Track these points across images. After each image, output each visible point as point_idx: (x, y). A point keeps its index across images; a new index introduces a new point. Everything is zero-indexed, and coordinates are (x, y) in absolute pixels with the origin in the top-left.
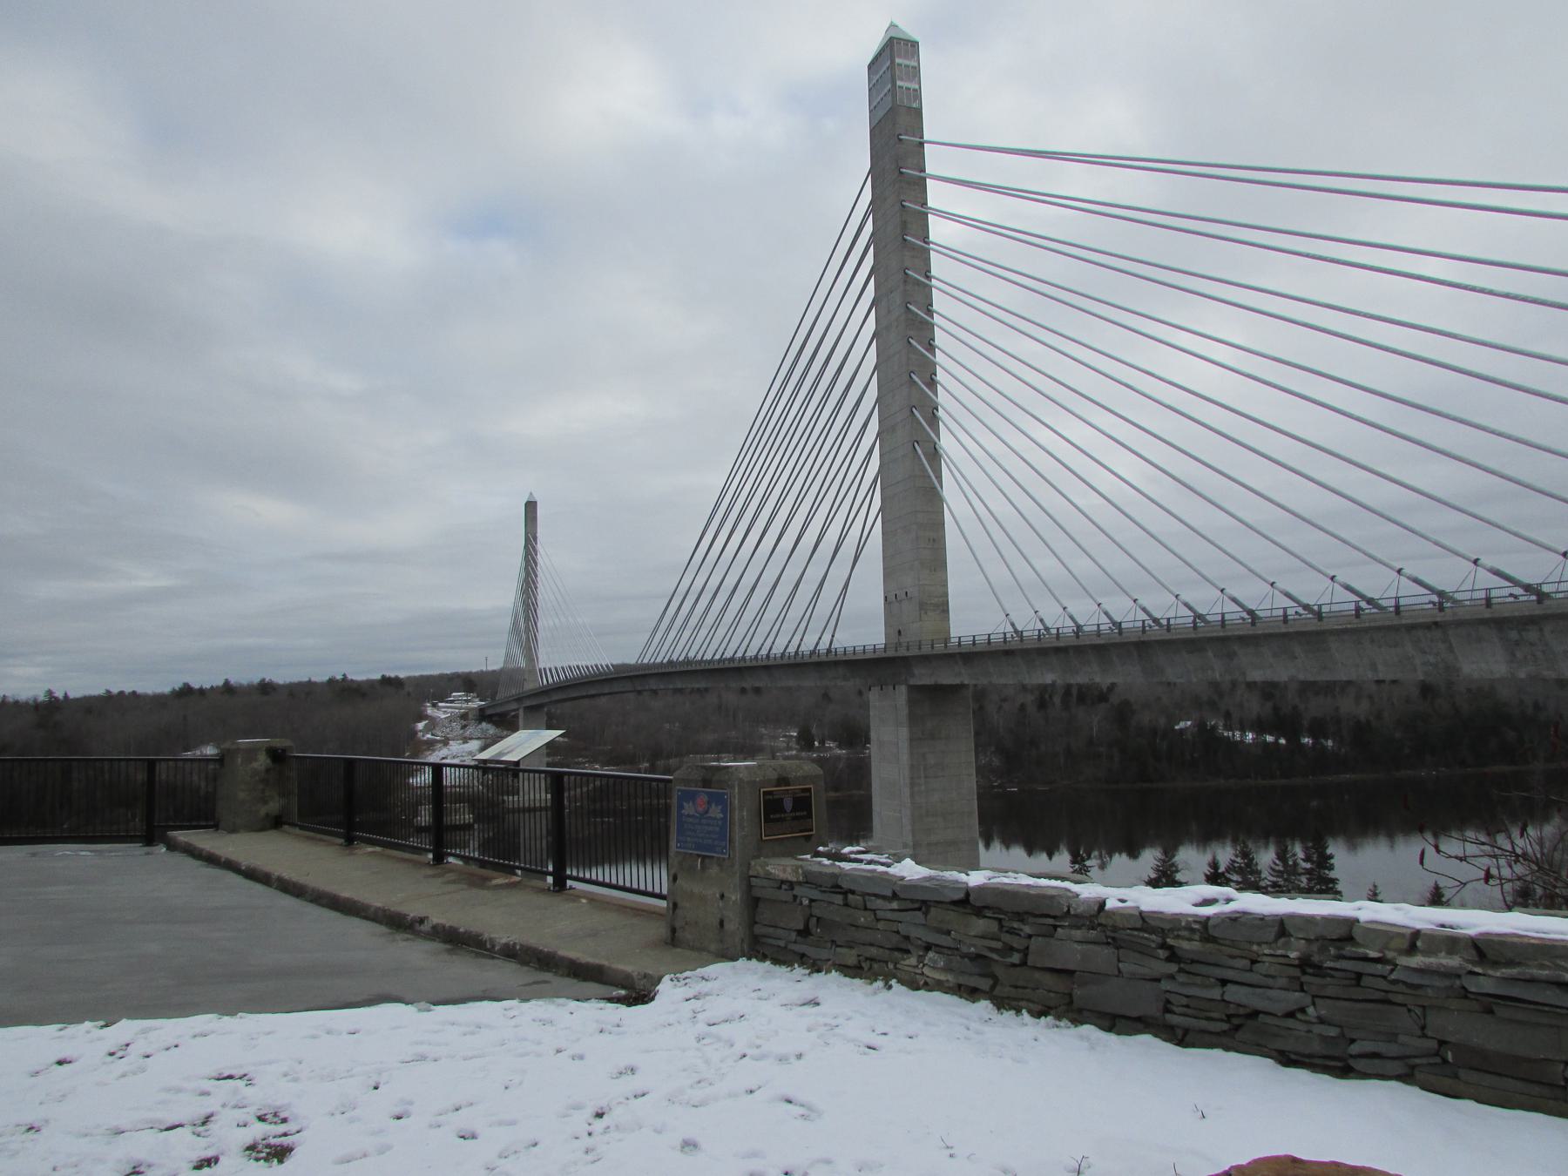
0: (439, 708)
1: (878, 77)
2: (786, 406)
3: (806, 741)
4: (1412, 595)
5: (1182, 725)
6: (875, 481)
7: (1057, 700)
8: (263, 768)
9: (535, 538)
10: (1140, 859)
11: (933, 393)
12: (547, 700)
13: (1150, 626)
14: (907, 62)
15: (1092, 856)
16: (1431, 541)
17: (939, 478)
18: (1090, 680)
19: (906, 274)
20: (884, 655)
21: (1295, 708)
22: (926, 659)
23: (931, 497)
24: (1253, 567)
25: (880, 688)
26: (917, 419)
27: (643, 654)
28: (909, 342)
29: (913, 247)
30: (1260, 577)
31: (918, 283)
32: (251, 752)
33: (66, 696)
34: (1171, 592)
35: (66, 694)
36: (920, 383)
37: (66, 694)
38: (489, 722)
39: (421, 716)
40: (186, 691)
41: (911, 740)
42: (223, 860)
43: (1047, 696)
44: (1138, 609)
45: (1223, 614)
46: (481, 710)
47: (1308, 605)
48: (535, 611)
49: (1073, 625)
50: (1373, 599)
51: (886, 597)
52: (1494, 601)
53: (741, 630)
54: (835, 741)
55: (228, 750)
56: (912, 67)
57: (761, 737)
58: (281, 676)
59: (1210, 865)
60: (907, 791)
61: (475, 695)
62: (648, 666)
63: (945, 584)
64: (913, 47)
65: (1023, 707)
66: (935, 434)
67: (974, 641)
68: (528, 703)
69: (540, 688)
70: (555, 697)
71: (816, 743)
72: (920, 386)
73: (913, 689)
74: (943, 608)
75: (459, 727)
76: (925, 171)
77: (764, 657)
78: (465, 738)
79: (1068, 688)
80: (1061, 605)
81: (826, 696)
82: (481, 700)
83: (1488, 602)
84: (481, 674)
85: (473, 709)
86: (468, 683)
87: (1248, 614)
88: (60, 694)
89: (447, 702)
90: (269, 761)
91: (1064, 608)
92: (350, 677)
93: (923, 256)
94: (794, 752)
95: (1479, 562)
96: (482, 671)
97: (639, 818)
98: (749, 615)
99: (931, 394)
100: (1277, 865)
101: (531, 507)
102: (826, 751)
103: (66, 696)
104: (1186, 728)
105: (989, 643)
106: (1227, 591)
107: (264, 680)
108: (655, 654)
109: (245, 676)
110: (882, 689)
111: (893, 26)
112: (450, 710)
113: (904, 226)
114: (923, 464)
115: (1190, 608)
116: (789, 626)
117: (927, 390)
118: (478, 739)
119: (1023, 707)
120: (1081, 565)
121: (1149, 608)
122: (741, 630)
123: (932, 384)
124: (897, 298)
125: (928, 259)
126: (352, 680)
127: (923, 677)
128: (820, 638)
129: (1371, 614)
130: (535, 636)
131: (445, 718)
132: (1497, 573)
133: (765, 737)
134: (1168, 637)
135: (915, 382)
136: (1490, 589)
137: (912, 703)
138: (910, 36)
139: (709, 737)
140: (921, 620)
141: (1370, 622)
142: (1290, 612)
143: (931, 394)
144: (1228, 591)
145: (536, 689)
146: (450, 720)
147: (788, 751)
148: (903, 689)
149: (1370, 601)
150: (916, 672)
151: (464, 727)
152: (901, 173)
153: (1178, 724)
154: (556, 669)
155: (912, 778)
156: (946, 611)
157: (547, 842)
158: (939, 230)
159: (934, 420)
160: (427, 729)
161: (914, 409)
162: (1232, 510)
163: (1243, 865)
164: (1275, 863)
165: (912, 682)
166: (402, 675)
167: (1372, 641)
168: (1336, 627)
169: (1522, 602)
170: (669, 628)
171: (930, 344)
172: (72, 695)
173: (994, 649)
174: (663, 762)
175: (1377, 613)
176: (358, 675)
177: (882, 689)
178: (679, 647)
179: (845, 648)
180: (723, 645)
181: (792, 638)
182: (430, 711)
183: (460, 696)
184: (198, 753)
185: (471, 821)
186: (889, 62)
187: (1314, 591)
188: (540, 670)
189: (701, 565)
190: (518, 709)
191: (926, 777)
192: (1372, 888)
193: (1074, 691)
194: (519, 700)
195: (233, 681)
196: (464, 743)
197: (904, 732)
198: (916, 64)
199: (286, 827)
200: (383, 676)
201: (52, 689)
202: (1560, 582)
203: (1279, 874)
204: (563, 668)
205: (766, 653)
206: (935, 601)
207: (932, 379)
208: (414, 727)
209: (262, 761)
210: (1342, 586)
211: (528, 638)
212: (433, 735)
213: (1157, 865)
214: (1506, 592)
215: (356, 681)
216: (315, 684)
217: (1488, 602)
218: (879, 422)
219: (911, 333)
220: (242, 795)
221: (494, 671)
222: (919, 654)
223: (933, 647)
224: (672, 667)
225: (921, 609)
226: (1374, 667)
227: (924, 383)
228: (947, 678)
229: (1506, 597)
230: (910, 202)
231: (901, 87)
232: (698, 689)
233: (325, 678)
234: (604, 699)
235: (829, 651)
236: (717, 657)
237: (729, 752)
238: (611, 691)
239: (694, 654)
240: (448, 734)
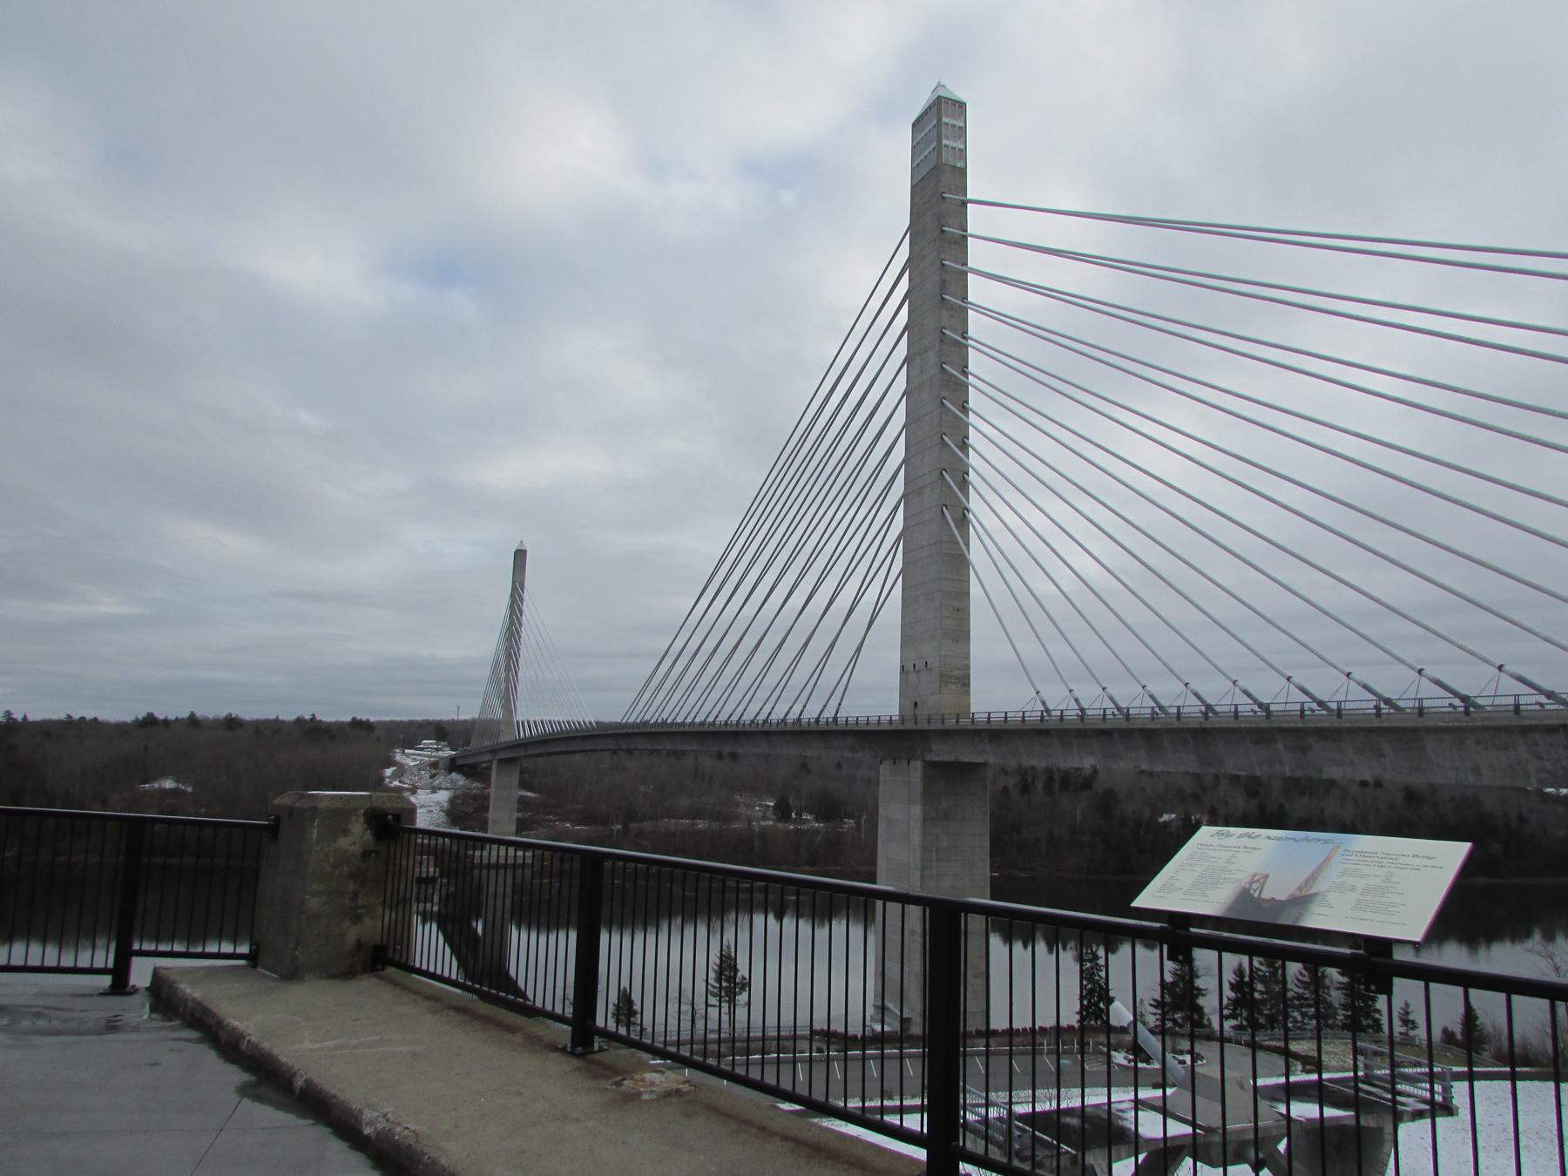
0: (408, 755)
1: (922, 135)
3: (783, 811)
4: (1438, 701)
5: (1166, 817)
6: (898, 540)
7: (1040, 786)
8: (357, 849)
9: (522, 587)
10: (1118, 952)
11: (965, 455)
13: (1313, 711)
17: (967, 545)
18: (1136, 766)
19: (943, 333)
22: (946, 734)
23: (959, 563)
24: (1218, 663)
29: (952, 307)
30: (1223, 673)
31: (956, 343)
32: (338, 818)
33: (25, 718)
35: (25, 716)
36: (951, 444)
37: (25, 716)
38: (459, 773)
40: (150, 722)
41: (925, 819)
42: (299, 1083)
43: (1029, 781)
46: (452, 759)
48: (517, 662)
49: (1113, 706)
52: (1425, 711)
53: (716, 694)
54: (811, 814)
55: (291, 811)
57: (737, 805)
58: (248, 713)
59: (1235, 973)
60: (918, 874)
61: (446, 743)
64: (960, 107)
65: (1005, 790)
68: (502, 756)
69: (516, 740)
70: (531, 751)
71: (793, 815)
72: (952, 449)
73: (930, 766)
74: (964, 682)
75: (428, 776)
76: (967, 231)
77: (830, 720)
78: (434, 787)
79: (1049, 772)
80: (1035, 689)
81: (804, 767)
82: (451, 750)
83: (1517, 708)
84: (453, 723)
85: (443, 758)
86: (441, 731)
87: (1259, 707)
88: (18, 716)
89: (417, 749)
90: (368, 836)
91: (1038, 693)
92: (318, 718)
93: (960, 314)
94: (771, 823)
96: (453, 720)
98: (723, 682)
101: (520, 556)
103: (25, 718)
106: (1190, 686)
107: (230, 715)
108: (628, 715)
109: (212, 710)
110: (895, 763)
111: (939, 86)
112: (419, 758)
113: (943, 285)
114: (951, 529)
115: (1249, 695)
117: (959, 453)
118: (447, 789)
119: (1005, 790)
120: (1058, 648)
121: (1116, 698)
122: (716, 694)
123: (964, 446)
124: (932, 357)
125: (965, 320)
126: (320, 721)
127: (942, 753)
128: (791, 708)
129: (1320, 715)
130: (515, 687)
133: (742, 805)
134: (1336, 723)
135: (947, 444)
136: (1518, 695)
137: (927, 780)
138: (955, 96)
139: (684, 802)
141: (1482, 721)
144: (1191, 685)
145: (512, 742)
146: (420, 768)
147: (764, 820)
148: (918, 764)
149: (1388, 701)
150: (934, 747)
151: (433, 776)
152: (943, 231)
153: (1162, 816)
155: (923, 860)
157: (513, 900)
158: (977, 290)
159: (964, 484)
160: (394, 776)
161: (944, 472)
162: (1200, 603)
163: (1267, 974)
164: (1301, 974)
165: (930, 757)
167: (1478, 742)
168: (1441, 724)
169: (1548, 710)
170: (674, 689)
171: (964, 407)
172: (31, 718)
175: (1326, 715)
176: (327, 716)
177: (895, 763)
178: (652, 709)
180: (696, 710)
182: (398, 757)
183: (431, 744)
184: (156, 785)
185: (437, 874)
186: (936, 121)
187: (1329, 687)
188: (518, 722)
190: (491, 761)
191: (938, 860)
192: (1403, 1005)
193: (1057, 777)
194: (493, 751)
195: (198, 714)
196: (432, 793)
197: (917, 811)
199: (391, 970)
200: (354, 719)
201: (10, 709)
203: (1305, 985)
204: (535, 722)
205: (737, 719)
207: (964, 442)
209: (358, 835)
210: (1296, 686)
211: (507, 688)
212: (400, 782)
213: (1176, 970)
215: (324, 722)
216: (283, 721)
217: (1517, 708)
219: (944, 394)
220: (314, 903)
221: (466, 721)
223: (957, 722)
226: (1476, 770)
227: (957, 446)
228: (968, 755)
231: (946, 146)
232: (675, 751)
233: (293, 717)
234: (578, 757)
235: (765, 721)
236: (689, 720)
237: (705, 819)
238: (593, 748)
239: (666, 716)
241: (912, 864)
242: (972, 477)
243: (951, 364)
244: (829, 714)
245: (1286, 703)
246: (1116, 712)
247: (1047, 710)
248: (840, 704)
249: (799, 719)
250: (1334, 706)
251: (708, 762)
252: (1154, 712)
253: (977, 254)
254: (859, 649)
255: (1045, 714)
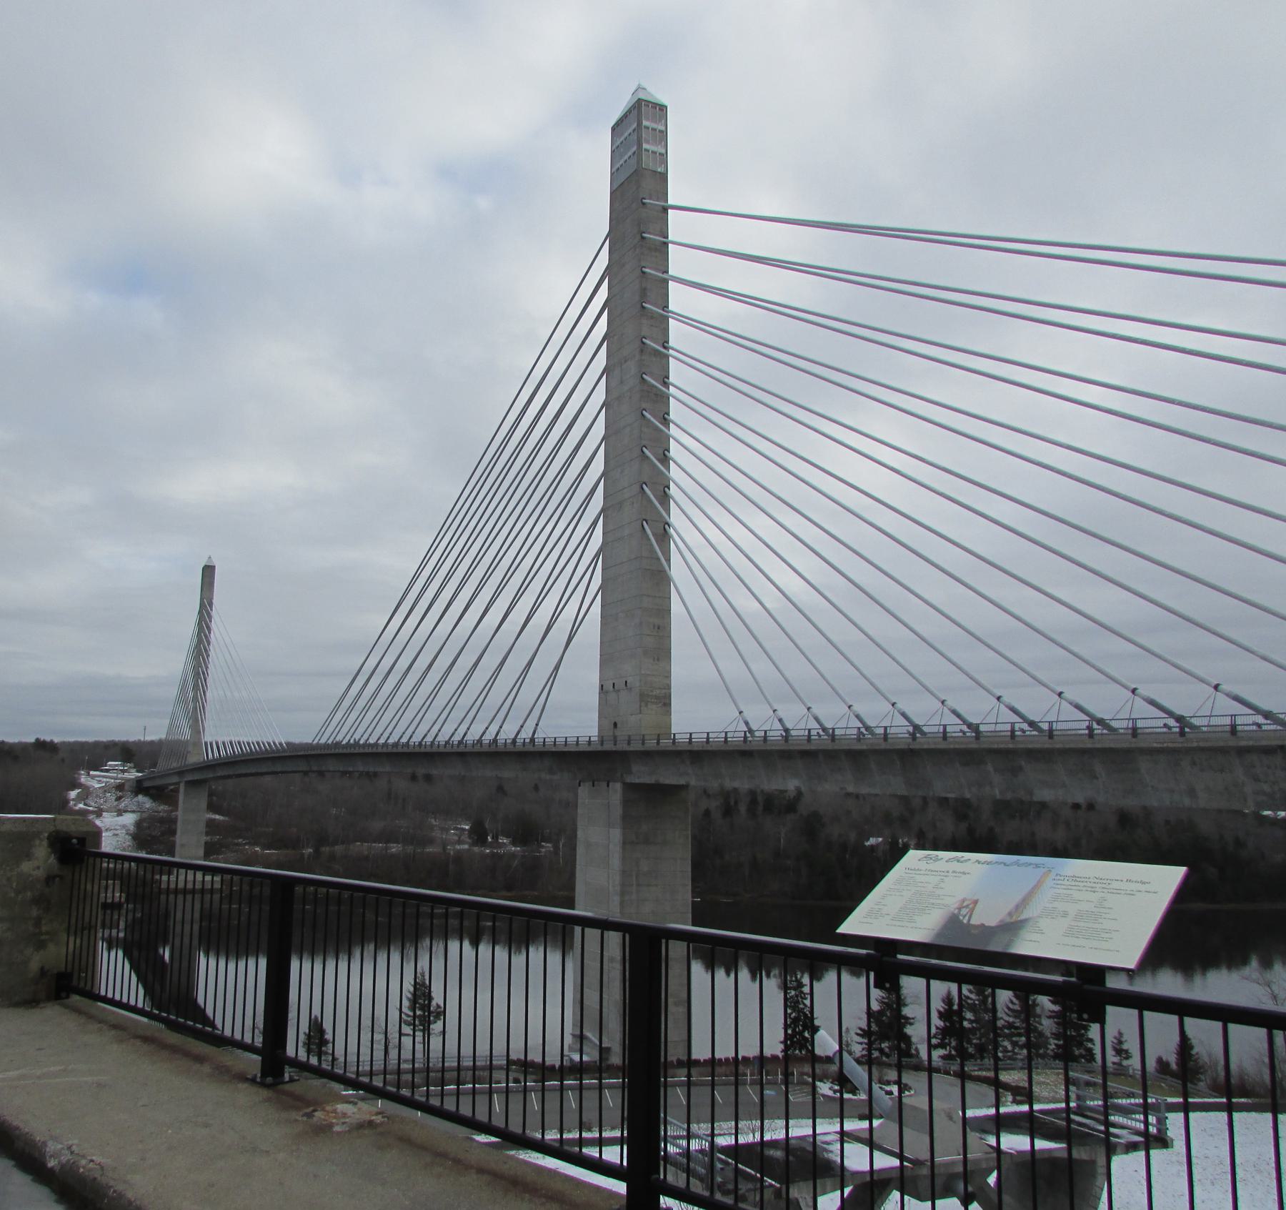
0: (93, 777)
1: (622, 139)
2: (498, 477)
3: (479, 835)
4: (1152, 721)
5: (872, 841)
6: (597, 556)
7: (743, 808)
8: (40, 874)
9: (211, 604)
12: (211, 775)
13: (1023, 731)
14: (655, 126)
15: (772, 974)
16: (1258, 656)
17: (668, 560)
20: (600, 748)
21: (991, 830)
22: (646, 755)
24: (927, 683)
25: (591, 783)
26: (649, 497)
27: (321, 732)
28: (643, 415)
29: (652, 316)
31: (656, 352)
34: (844, 701)
39: (75, 785)
44: (896, 713)
45: (945, 726)
46: (139, 781)
47: (1103, 719)
48: (205, 681)
49: (818, 727)
50: (1183, 717)
51: (602, 686)
52: (1139, 731)
53: (409, 715)
54: (507, 837)
56: (660, 131)
59: (943, 1001)
60: (617, 899)
61: (132, 765)
62: (326, 746)
63: (668, 675)
65: (707, 813)
66: (666, 513)
67: (708, 738)
68: (189, 777)
70: (220, 773)
73: (630, 788)
74: (665, 702)
76: (668, 237)
81: (500, 789)
82: (138, 772)
83: (1233, 729)
84: (139, 744)
85: (129, 780)
86: (127, 752)
89: (102, 771)
91: (741, 713)
93: (661, 323)
94: (466, 847)
95: (1137, 692)
96: (140, 740)
97: (307, 907)
99: (665, 471)
100: (1015, 1004)
101: (208, 571)
102: (500, 847)
104: (878, 845)
105: (708, 742)
111: (639, 88)
112: (105, 780)
113: (643, 293)
116: (457, 714)
118: (133, 812)
120: (762, 667)
122: (409, 715)
123: (665, 459)
124: (632, 367)
127: (641, 774)
129: (1030, 736)
131: (100, 788)
132: (1152, 703)
135: (647, 457)
137: (626, 803)
139: (377, 825)
140: (640, 713)
142: (814, 733)
143: (665, 471)
145: (199, 763)
146: (105, 790)
147: (459, 844)
148: (618, 786)
149: (1100, 722)
150: (635, 768)
151: (119, 799)
154: (224, 743)
156: (667, 705)
158: (678, 298)
159: (665, 498)
160: (79, 798)
161: (644, 486)
163: (977, 1002)
164: (1012, 1002)
165: (629, 779)
166: (56, 740)
167: (1194, 763)
168: (1155, 745)
171: (665, 419)
173: (508, 750)
174: (328, 849)
179: (545, 739)
181: (442, 727)
182: (83, 779)
183: (117, 765)
188: (206, 743)
189: (390, 644)
190: (178, 783)
191: (638, 885)
192: (1117, 1035)
193: (760, 799)
194: (180, 773)
196: (118, 816)
197: (616, 834)
198: (663, 128)
200: (37, 740)
202: (996, 723)
203: (1016, 1014)
206: (657, 692)
207: (664, 455)
208: (66, 796)
209: (41, 860)
211: (195, 708)
212: (85, 804)
213: (883, 998)
214: (957, 728)
217: (1233, 729)
218: (604, 498)
219: (644, 405)
221: (152, 742)
222: (643, 749)
223: (658, 743)
224: (328, 749)
225: (641, 701)
226: (1192, 792)
228: (668, 777)
229: (1250, 725)
230: (650, 268)
232: (368, 773)
234: (268, 778)
235: (460, 742)
236: (382, 741)
240: (102, 805)
241: (611, 888)
242: (673, 490)
243: (652, 375)
244: (526, 734)
245: (1210, 716)
246: (821, 733)
247: (751, 731)
248: (537, 725)
249: (495, 740)
250: (1045, 727)
251: (401, 785)
252: (860, 733)
253: (679, 262)
254: (557, 668)
255: (748, 735)
